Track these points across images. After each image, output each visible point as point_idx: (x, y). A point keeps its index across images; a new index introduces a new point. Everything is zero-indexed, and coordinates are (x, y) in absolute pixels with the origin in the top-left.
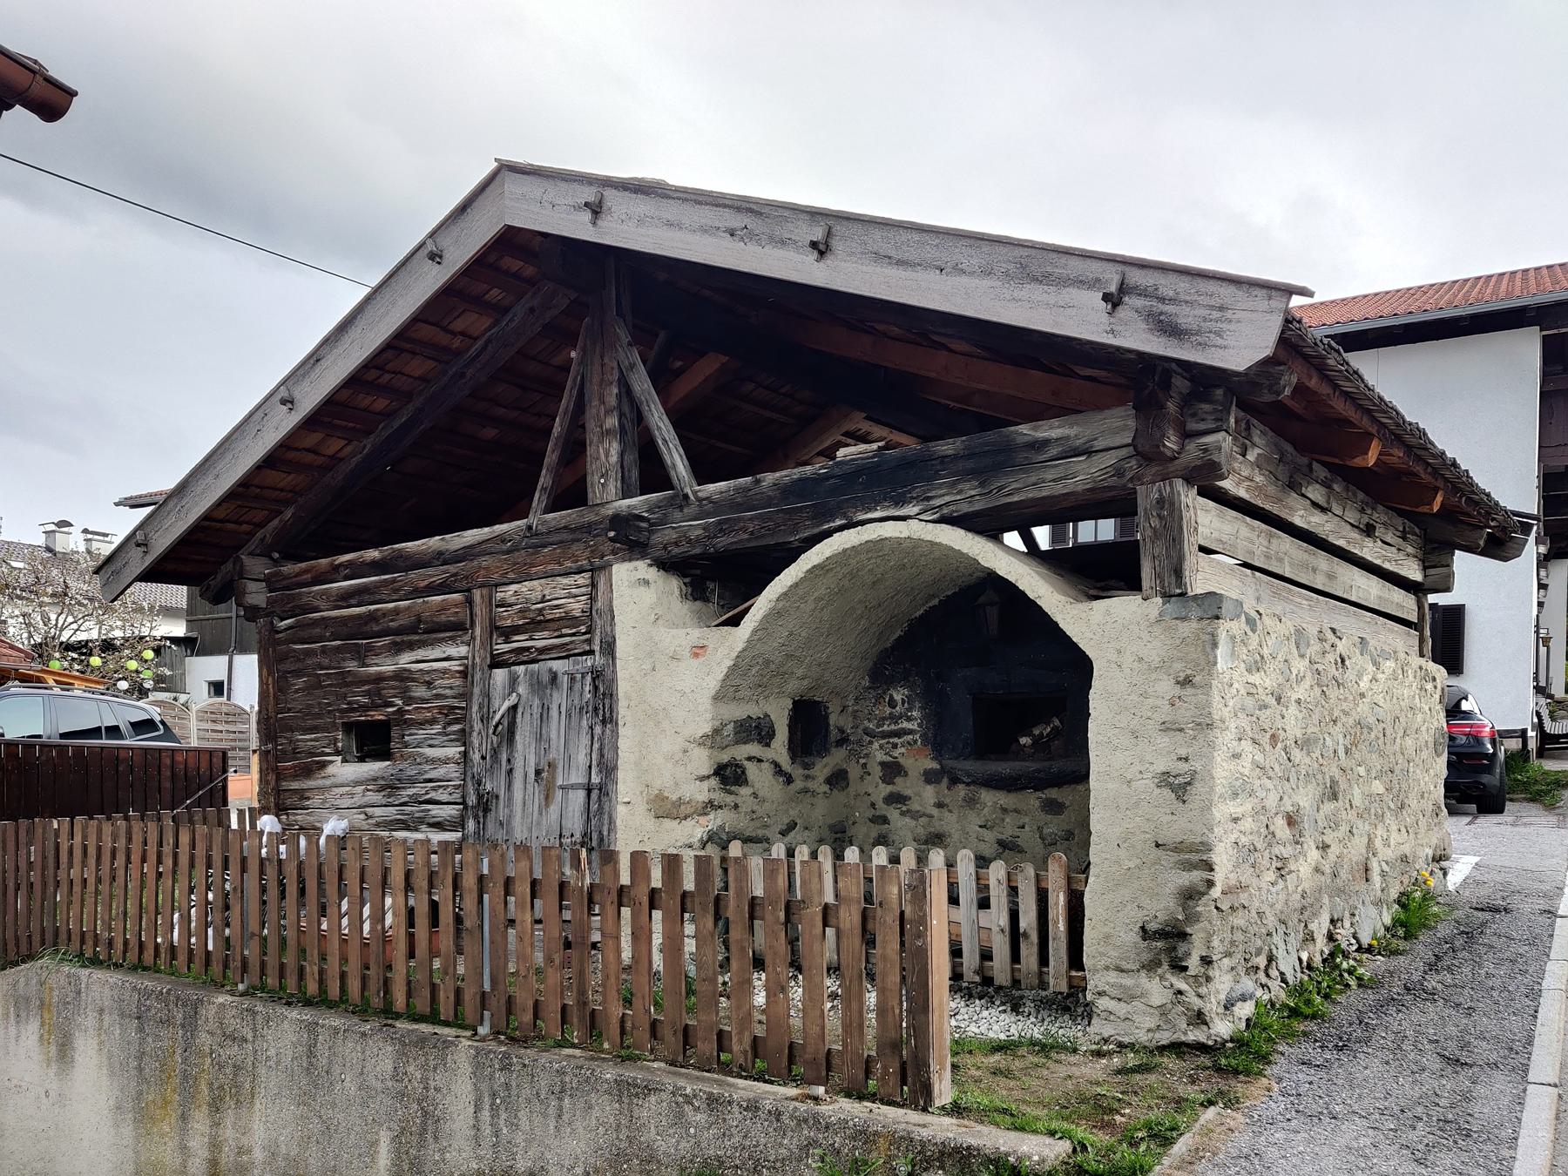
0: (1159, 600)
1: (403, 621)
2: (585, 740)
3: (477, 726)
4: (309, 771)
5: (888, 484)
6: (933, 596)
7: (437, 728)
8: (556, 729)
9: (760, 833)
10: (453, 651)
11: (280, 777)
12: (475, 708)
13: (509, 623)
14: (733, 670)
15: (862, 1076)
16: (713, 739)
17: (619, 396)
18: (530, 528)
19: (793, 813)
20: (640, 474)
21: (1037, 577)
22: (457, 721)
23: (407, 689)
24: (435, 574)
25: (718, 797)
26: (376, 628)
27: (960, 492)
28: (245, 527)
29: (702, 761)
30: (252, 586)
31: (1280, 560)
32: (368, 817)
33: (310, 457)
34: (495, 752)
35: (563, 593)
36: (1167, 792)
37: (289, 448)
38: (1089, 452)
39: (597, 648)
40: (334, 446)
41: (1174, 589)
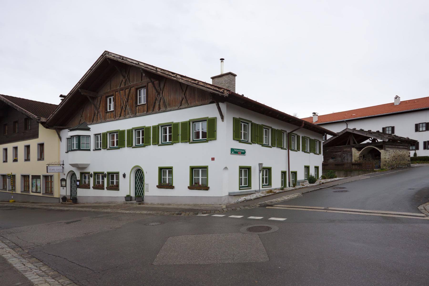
35: (349, 149)
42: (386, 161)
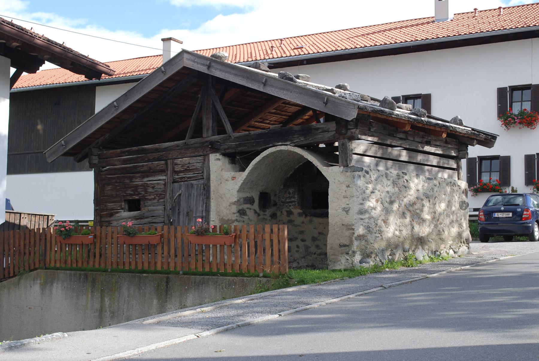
1: (145, 168)
2: (201, 203)
4: (111, 215)
6: (300, 162)
7: (155, 201)
10: (161, 178)
11: (101, 217)
12: (168, 194)
13: (178, 170)
14: (242, 183)
16: (237, 203)
18: (185, 143)
22: (163, 198)
23: (146, 189)
24: (156, 155)
29: (234, 209)
30: (94, 157)
35: (196, 162)
36: (345, 213)
38: (328, 131)
39: (205, 177)
41: (346, 166)
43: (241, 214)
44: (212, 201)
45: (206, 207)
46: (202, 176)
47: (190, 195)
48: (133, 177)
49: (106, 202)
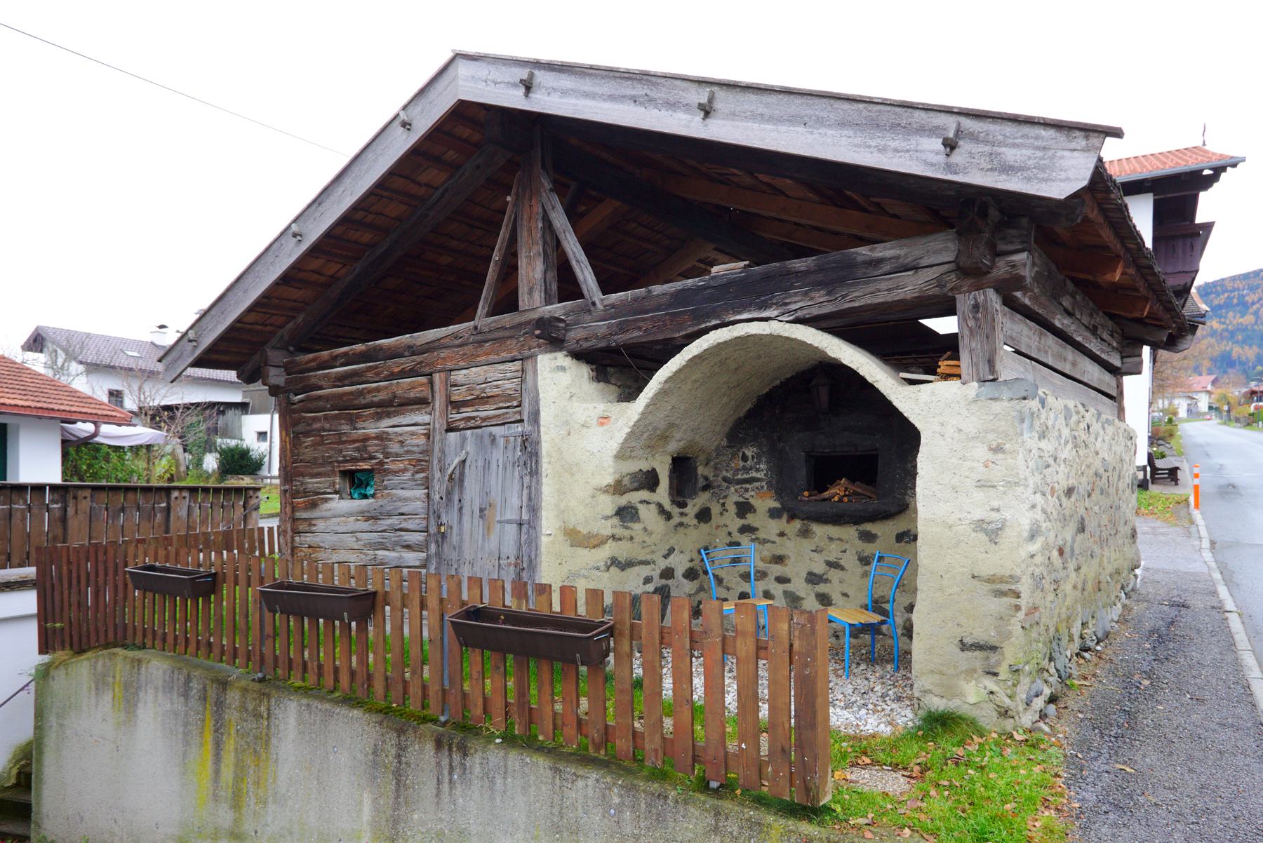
0: (975, 384)
1: (382, 396)
2: (517, 486)
3: (438, 475)
4: (314, 505)
5: (749, 295)
6: (776, 379)
7: (408, 475)
8: (494, 482)
9: (649, 557)
12: (435, 462)
14: (631, 435)
15: (755, 777)
16: (618, 488)
17: (544, 228)
18: (476, 328)
19: (673, 542)
20: (559, 287)
21: (874, 366)
22: (423, 470)
23: (386, 447)
24: (407, 363)
25: (620, 532)
26: (363, 402)
27: (812, 299)
28: (269, 328)
29: (608, 504)
31: (1046, 352)
32: (358, 540)
33: (315, 277)
34: (449, 493)
35: (490, 375)
36: (982, 536)
37: (300, 270)
38: (916, 268)
39: (525, 417)
40: (333, 268)
42: (1003, 587)
43: (623, 519)
44: (544, 480)
45: (530, 499)
46: (520, 413)
47: (487, 465)
48: (358, 416)
49: (303, 475)
